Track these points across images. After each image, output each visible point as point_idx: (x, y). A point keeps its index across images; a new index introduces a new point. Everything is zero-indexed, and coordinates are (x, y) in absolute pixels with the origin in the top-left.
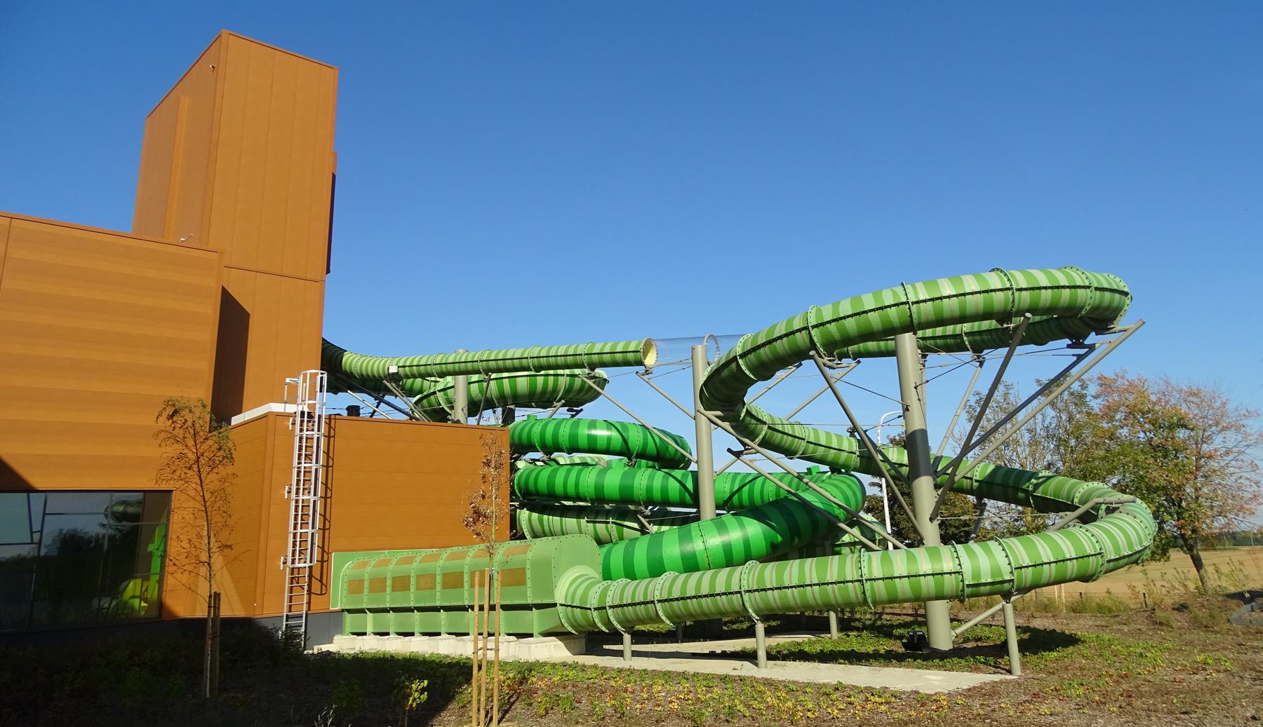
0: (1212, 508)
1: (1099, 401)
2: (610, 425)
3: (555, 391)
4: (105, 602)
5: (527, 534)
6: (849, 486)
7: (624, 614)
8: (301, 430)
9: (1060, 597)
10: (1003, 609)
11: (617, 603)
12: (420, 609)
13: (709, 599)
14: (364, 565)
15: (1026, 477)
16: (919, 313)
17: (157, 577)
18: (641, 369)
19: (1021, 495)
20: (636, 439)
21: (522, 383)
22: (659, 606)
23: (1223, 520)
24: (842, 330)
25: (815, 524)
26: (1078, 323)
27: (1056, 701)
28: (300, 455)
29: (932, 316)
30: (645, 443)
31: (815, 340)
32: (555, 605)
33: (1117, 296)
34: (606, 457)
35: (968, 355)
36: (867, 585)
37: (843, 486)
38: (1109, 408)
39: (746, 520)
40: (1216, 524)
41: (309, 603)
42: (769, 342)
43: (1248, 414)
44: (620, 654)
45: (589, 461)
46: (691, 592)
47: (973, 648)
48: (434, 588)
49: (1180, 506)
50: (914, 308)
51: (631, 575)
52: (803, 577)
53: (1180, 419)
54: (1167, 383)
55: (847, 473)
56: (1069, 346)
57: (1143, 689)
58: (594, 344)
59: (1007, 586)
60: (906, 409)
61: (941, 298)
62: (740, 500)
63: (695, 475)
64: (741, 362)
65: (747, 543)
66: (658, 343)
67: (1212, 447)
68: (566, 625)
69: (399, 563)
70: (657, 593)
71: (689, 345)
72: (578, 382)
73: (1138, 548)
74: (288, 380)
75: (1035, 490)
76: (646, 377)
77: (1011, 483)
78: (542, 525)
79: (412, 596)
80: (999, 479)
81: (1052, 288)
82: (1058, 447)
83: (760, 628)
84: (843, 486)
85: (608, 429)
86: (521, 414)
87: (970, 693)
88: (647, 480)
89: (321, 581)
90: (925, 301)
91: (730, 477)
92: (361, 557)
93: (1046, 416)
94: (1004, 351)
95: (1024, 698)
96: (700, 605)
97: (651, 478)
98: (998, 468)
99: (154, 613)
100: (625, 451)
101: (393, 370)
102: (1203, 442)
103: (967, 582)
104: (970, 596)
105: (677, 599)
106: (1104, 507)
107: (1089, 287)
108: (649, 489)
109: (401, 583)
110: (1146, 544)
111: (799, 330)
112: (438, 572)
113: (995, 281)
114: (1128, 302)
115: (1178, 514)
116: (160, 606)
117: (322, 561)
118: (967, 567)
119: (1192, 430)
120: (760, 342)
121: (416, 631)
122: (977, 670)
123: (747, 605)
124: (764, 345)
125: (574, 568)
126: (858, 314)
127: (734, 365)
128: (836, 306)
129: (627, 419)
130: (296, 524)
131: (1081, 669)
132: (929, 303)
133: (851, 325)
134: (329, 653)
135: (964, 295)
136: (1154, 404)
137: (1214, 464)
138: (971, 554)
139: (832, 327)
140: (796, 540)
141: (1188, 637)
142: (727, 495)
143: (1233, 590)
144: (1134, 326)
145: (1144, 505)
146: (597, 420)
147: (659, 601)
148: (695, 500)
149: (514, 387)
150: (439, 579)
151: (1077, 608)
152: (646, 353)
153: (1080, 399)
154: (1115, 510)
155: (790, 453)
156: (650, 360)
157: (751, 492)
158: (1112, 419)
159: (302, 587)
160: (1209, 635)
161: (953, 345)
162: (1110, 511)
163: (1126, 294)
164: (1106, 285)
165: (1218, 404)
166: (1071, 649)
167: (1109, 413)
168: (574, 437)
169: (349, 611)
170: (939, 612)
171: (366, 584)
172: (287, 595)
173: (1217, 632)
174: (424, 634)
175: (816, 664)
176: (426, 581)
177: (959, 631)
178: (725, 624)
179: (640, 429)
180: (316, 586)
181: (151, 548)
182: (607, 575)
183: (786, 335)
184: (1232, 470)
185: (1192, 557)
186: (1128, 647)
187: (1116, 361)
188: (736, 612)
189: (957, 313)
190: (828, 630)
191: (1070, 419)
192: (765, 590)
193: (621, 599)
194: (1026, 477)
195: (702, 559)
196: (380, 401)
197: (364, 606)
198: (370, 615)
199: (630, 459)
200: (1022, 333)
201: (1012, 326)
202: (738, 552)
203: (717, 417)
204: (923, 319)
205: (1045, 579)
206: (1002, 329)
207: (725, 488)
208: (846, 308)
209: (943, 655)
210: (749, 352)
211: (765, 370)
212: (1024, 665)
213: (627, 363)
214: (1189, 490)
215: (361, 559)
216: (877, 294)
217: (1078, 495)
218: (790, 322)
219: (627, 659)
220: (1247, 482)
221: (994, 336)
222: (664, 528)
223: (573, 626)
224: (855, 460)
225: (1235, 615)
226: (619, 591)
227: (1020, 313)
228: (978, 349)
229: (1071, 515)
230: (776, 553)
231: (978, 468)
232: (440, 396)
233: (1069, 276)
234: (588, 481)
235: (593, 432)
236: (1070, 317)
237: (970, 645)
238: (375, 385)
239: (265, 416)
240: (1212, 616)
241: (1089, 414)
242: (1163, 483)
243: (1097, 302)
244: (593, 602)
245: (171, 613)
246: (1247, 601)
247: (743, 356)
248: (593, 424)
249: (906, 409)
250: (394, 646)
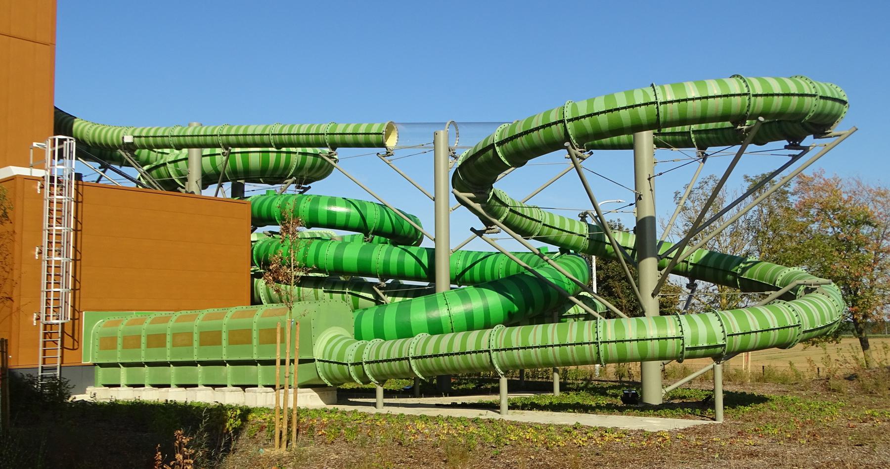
0: (884, 296)
1: (796, 197)
2: (349, 203)
3: (287, 167)
5: (263, 301)
6: (579, 266)
7: (379, 368)
8: (51, 194)
9: (746, 368)
10: (713, 369)
12: (176, 364)
13: (460, 357)
14: (117, 323)
15: (735, 261)
16: (665, 113)
18: (382, 151)
19: (730, 277)
20: (373, 216)
21: (255, 158)
22: (412, 362)
24: (595, 125)
25: (547, 297)
26: (795, 126)
27: (756, 438)
29: (676, 116)
30: (382, 221)
31: (570, 132)
32: (313, 360)
33: (837, 104)
34: (347, 234)
35: (693, 152)
36: (602, 347)
37: (578, 261)
38: (804, 204)
41: (62, 357)
42: (526, 133)
44: (374, 405)
45: (325, 237)
46: (443, 350)
47: (679, 404)
49: (856, 295)
50: (661, 108)
51: (379, 334)
53: (866, 217)
54: (859, 184)
55: (576, 253)
56: (786, 147)
57: (824, 431)
59: (719, 350)
60: (639, 198)
61: (686, 100)
62: (472, 275)
63: (432, 253)
64: (497, 149)
66: (400, 127)
68: (323, 378)
69: (154, 322)
70: (412, 351)
74: (35, 144)
75: (742, 273)
76: (387, 159)
77: (722, 266)
78: (299, 293)
79: (168, 352)
80: (711, 263)
81: (783, 95)
84: (578, 261)
85: (347, 206)
86: (251, 189)
87: (686, 431)
88: (383, 254)
89: (73, 337)
90: (671, 102)
91: (463, 255)
92: (113, 316)
93: (751, 208)
94: (737, 148)
96: (451, 362)
97: (389, 253)
98: (711, 254)
100: (363, 228)
101: (128, 139)
102: (883, 238)
103: (686, 346)
106: (802, 288)
107: (815, 96)
108: (386, 263)
109: (157, 340)
110: (835, 319)
113: (735, 86)
114: (845, 110)
115: (853, 301)
117: (73, 319)
119: (876, 227)
121: (172, 383)
122: (686, 417)
123: (495, 362)
124: (521, 135)
125: (333, 331)
127: (490, 152)
128: (591, 102)
129: (365, 197)
130: (49, 283)
131: (772, 418)
132: (676, 104)
133: (603, 121)
134: (83, 402)
135: (707, 98)
136: (845, 202)
138: (692, 323)
139: (586, 122)
140: (531, 310)
141: (856, 399)
142: (459, 271)
144: (848, 132)
145: (836, 287)
146: (332, 194)
147: (414, 358)
148: (431, 274)
149: (246, 163)
150: (196, 337)
151: (763, 377)
152: (387, 135)
154: (813, 290)
155: (526, 233)
157: (482, 269)
158: (807, 214)
159: (55, 342)
160: (874, 398)
161: (683, 142)
162: (809, 291)
163: (844, 103)
164: (829, 95)
166: (761, 405)
167: (804, 207)
168: (313, 212)
169: (102, 365)
171: (120, 341)
172: (41, 348)
173: (880, 397)
174: (180, 386)
175: (549, 413)
176: (183, 338)
177: (668, 389)
178: (453, 384)
180: (68, 341)
182: (358, 336)
183: (543, 127)
187: (833, 165)
189: (699, 114)
190: (552, 390)
191: (771, 212)
192: (511, 349)
193: (377, 354)
194: (735, 261)
195: (446, 325)
197: (118, 361)
198: (123, 370)
199: (366, 235)
200: (752, 134)
201: (745, 127)
202: (479, 318)
203: (470, 198)
204: (669, 118)
205: (751, 344)
206: (733, 129)
207: (459, 264)
208: (600, 105)
209: (656, 408)
210: (507, 140)
211: (519, 158)
212: (725, 415)
213: (369, 145)
214: (865, 280)
215: (112, 319)
216: (629, 93)
217: (780, 278)
221: (720, 135)
223: (329, 379)
224: (584, 243)
226: (371, 349)
227: (754, 116)
229: (774, 294)
230: (511, 320)
231: (694, 255)
232: (170, 167)
233: (783, 84)
234: (328, 254)
235: (333, 209)
236: (795, 122)
237: (677, 401)
238: (102, 153)
239: (13, 179)
241: (787, 209)
242: (844, 274)
243: (820, 109)
244: (350, 358)
247: (500, 144)
248: (332, 201)
249: (639, 198)
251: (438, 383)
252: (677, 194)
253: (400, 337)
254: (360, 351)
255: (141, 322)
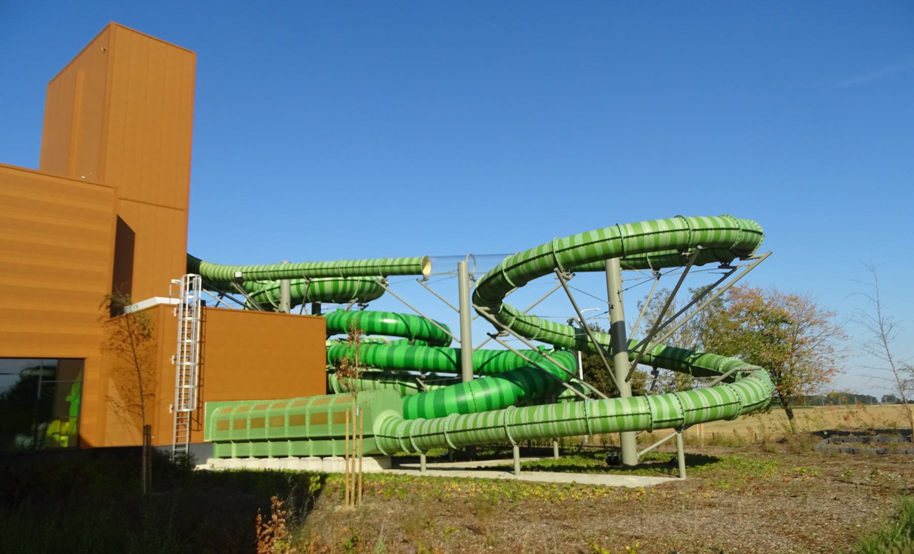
0: (801, 377)
2: (397, 316)
3: (351, 291)
4: (23, 441)
8: (184, 316)
11: (417, 434)
14: (230, 410)
15: (687, 354)
16: (628, 245)
17: (75, 419)
18: (420, 277)
20: (415, 326)
21: (329, 285)
23: (808, 386)
25: (546, 383)
26: (726, 252)
28: (183, 334)
29: (636, 246)
30: (421, 329)
32: (373, 436)
33: (756, 235)
35: (650, 272)
36: (589, 422)
37: (565, 359)
39: (500, 380)
40: (803, 388)
41: (190, 437)
42: (526, 262)
43: (829, 314)
45: (380, 342)
48: (283, 425)
49: (780, 376)
50: (625, 241)
51: (422, 414)
52: (543, 416)
54: (776, 292)
56: (719, 267)
57: (765, 485)
58: (387, 259)
59: (679, 422)
60: (611, 307)
61: (643, 235)
62: (489, 368)
63: (459, 352)
64: (505, 274)
65: (501, 396)
67: (804, 336)
68: (380, 449)
71: (456, 261)
72: (368, 285)
73: (762, 399)
74: (173, 281)
76: (424, 283)
79: (267, 432)
80: (669, 355)
82: (701, 335)
83: (516, 450)
84: (565, 359)
85: (396, 318)
87: (658, 487)
88: (423, 354)
89: (198, 421)
90: (632, 236)
92: (242, 403)
94: (684, 268)
95: (691, 490)
97: (427, 352)
98: (668, 348)
99: (74, 444)
100: (408, 335)
101: (238, 275)
104: (656, 428)
105: (460, 431)
106: (739, 373)
108: (425, 361)
109: (258, 422)
110: (767, 396)
111: (547, 254)
112: (287, 414)
113: (678, 224)
115: (778, 381)
116: (77, 439)
117: (198, 408)
118: (654, 410)
120: (519, 261)
122: (656, 475)
123: (509, 434)
124: (522, 263)
125: (387, 413)
126: (588, 244)
127: (500, 277)
128: (572, 238)
129: (409, 312)
130: (181, 382)
131: (724, 475)
133: (582, 251)
134: (205, 471)
135: (658, 233)
136: (767, 306)
137: (804, 348)
138: (657, 402)
140: (534, 394)
141: (787, 458)
142: (480, 365)
143: (815, 430)
144: (765, 255)
146: (385, 310)
149: (322, 289)
150: (287, 420)
151: (714, 441)
152: (424, 266)
153: (718, 302)
154: (747, 375)
155: (528, 336)
156: (427, 271)
157: (497, 363)
159: (185, 426)
162: (745, 375)
163: (761, 234)
164: (749, 228)
165: (809, 307)
166: (714, 465)
167: (736, 311)
168: (371, 324)
169: (218, 442)
170: (630, 439)
172: (175, 430)
176: (277, 421)
179: (418, 319)
181: (68, 399)
182: (406, 416)
183: (538, 257)
184: (816, 352)
185: (787, 410)
186: (751, 463)
187: (750, 277)
188: (501, 439)
189: (653, 245)
190: (552, 455)
191: (711, 315)
192: (521, 425)
193: (420, 430)
194: (687, 354)
195: (471, 406)
196: (222, 295)
198: (234, 445)
199: (410, 339)
200: (694, 258)
201: (688, 254)
202: (496, 401)
205: (704, 417)
207: (479, 360)
208: (579, 240)
211: (521, 280)
212: (687, 473)
213: (410, 273)
214: (786, 365)
217: (722, 366)
218: (540, 248)
219: (424, 471)
220: (826, 361)
222: (442, 387)
223: (386, 450)
224: (572, 342)
225: (817, 446)
226: (416, 426)
227: (695, 245)
228: (656, 267)
230: (520, 402)
232: (268, 294)
233: (726, 222)
234: (382, 354)
235: (386, 321)
237: (649, 462)
238: (220, 285)
240: (802, 446)
241: (723, 313)
242: (770, 360)
244: (400, 433)
245: (86, 443)
246: (825, 437)
247: (507, 270)
248: (385, 315)
249: (611, 307)
250: (253, 465)
251: (466, 451)
252: (639, 303)
253: (437, 417)
254: (408, 428)
255: (247, 409)
